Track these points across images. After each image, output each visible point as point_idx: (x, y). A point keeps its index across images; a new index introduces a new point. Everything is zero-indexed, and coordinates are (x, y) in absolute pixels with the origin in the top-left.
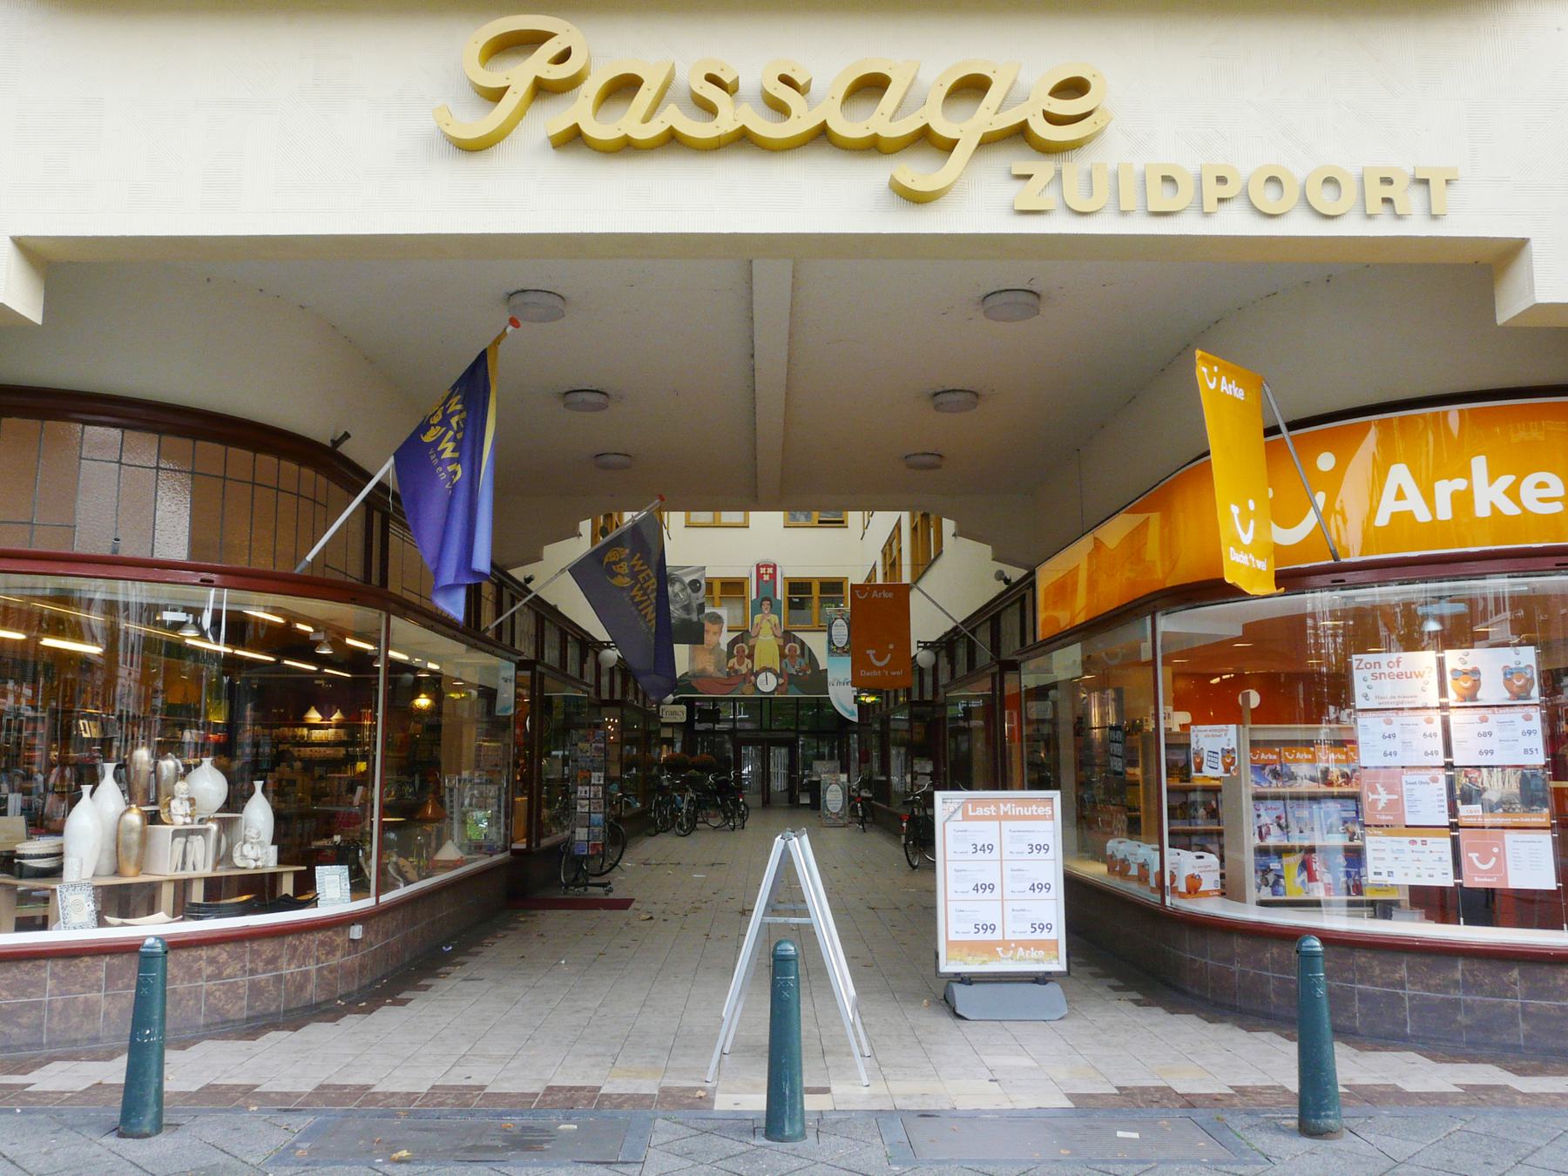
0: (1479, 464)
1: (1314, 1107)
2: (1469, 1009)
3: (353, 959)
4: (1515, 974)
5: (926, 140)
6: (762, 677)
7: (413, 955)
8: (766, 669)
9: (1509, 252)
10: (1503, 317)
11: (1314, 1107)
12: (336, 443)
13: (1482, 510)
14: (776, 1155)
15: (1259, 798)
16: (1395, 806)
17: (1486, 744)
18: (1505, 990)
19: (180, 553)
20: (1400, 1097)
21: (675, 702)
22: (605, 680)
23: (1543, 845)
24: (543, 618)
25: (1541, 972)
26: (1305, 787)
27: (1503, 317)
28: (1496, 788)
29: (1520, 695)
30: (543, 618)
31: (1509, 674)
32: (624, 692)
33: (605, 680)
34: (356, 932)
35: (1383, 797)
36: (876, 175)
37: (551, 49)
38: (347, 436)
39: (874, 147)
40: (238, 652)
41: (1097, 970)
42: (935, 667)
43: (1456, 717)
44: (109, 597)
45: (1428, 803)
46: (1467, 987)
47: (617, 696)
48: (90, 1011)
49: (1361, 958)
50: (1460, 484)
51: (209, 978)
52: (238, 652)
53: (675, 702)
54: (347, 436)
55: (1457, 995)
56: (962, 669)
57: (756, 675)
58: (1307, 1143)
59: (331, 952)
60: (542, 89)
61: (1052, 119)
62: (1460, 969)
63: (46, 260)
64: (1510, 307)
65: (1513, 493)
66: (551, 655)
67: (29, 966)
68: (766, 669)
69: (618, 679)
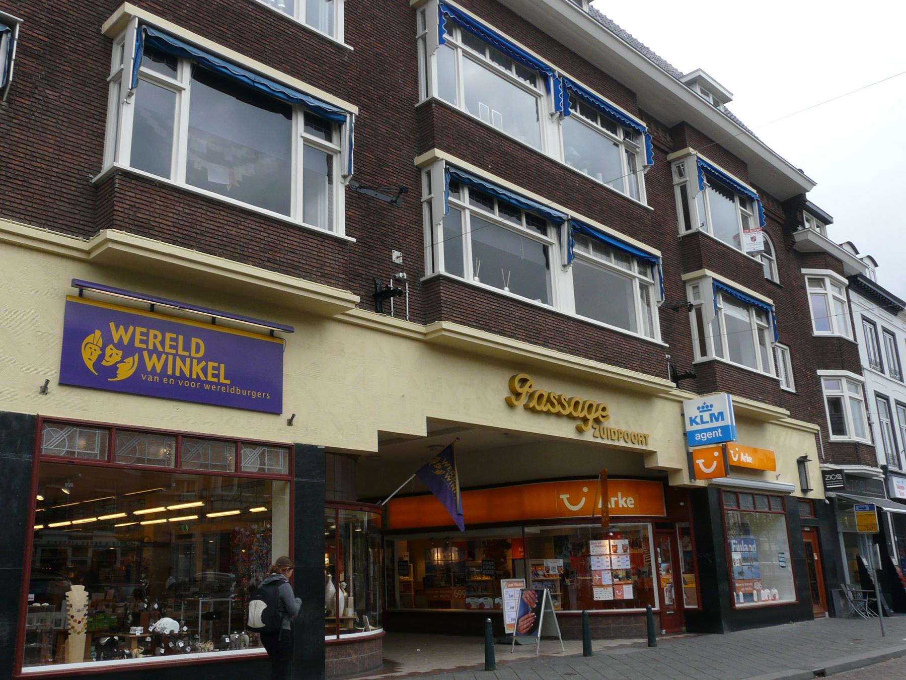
0: (619, 494)
13: (620, 506)
16: (600, 580)
17: (620, 563)
19: (274, 482)
23: (630, 587)
26: (542, 578)
28: (622, 574)
29: (625, 551)
31: (623, 546)
35: (598, 578)
40: (94, 519)
43: (613, 557)
44: (748, 537)
45: (607, 579)
49: (600, 619)
50: (616, 499)
52: (94, 519)
58: (651, 648)
62: (622, 619)
64: (649, 464)
65: (626, 502)
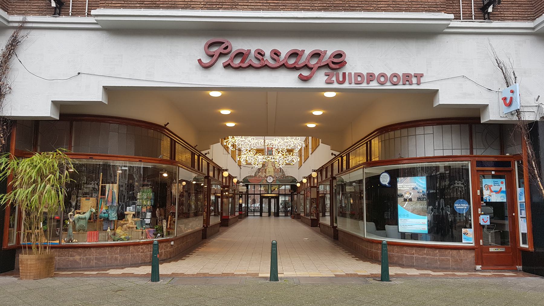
1: (385, 276)
2: (427, 259)
3: (171, 250)
4: (437, 251)
5: (306, 67)
6: (269, 178)
7: (186, 248)
8: (270, 176)
9: (435, 92)
10: (434, 106)
11: (385, 276)
12: (166, 125)
14: (274, 239)
15: (521, 218)
18: (435, 255)
20: (406, 275)
21: (243, 186)
22: (224, 180)
24: (194, 154)
25: (443, 251)
27: (434, 106)
30: (194, 154)
32: (229, 183)
33: (224, 180)
34: (172, 243)
36: (296, 74)
37: (224, 46)
38: (168, 123)
39: (294, 68)
41: (353, 256)
42: (317, 177)
46: (427, 254)
47: (227, 184)
48: (116, 259)
49: (405, 248)
51: (141, 252)
53: (243, 186)
54: (168, 123)
55: (424, 256)
56: (324, 178)
57: (267, 177)
59: (167, 248)
60: (221, 55)
61: (333, 63)
63: (107, 90)
66: (211, 174)
67: (102, 249)
68: (270, 176)
69: (227, 179)
